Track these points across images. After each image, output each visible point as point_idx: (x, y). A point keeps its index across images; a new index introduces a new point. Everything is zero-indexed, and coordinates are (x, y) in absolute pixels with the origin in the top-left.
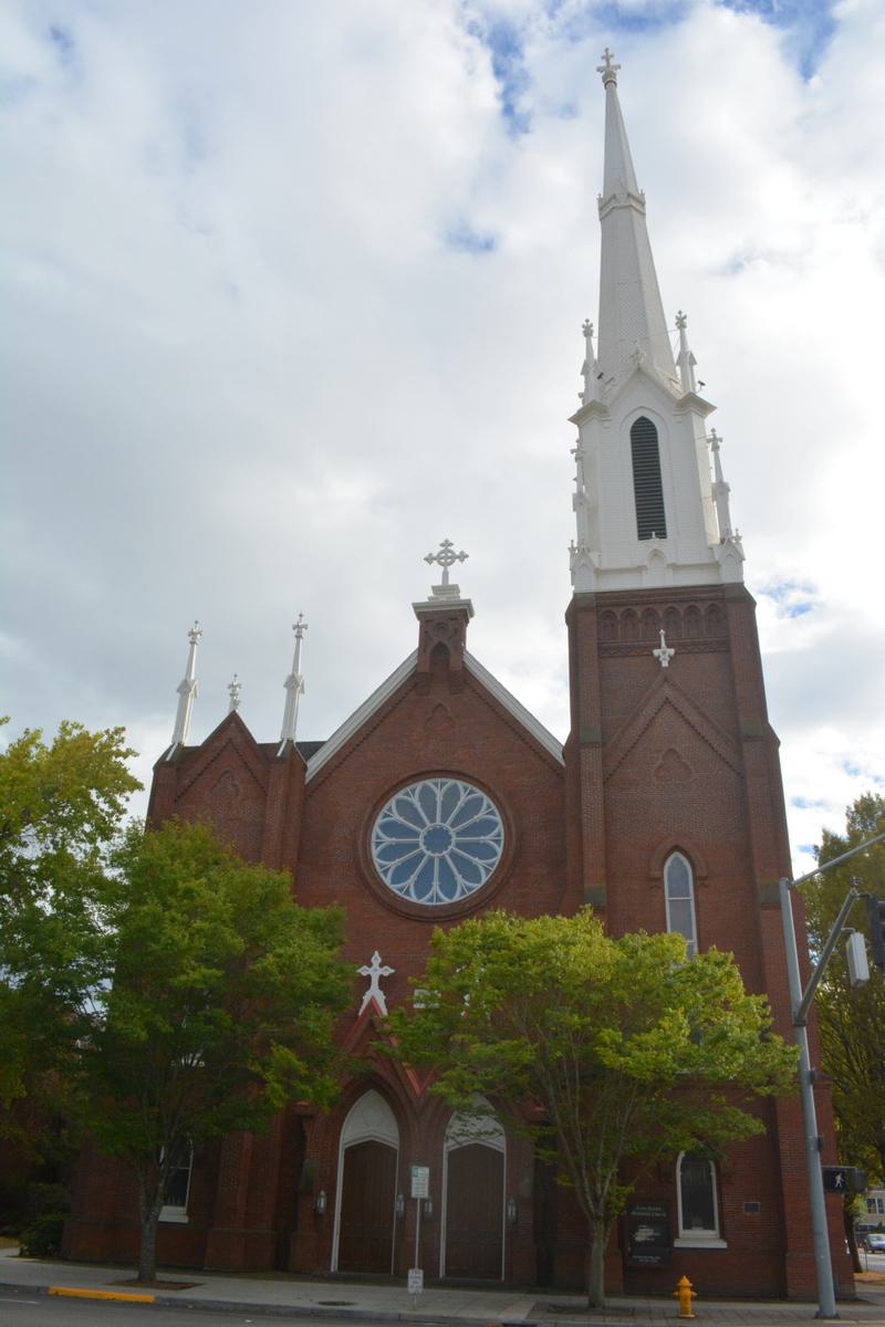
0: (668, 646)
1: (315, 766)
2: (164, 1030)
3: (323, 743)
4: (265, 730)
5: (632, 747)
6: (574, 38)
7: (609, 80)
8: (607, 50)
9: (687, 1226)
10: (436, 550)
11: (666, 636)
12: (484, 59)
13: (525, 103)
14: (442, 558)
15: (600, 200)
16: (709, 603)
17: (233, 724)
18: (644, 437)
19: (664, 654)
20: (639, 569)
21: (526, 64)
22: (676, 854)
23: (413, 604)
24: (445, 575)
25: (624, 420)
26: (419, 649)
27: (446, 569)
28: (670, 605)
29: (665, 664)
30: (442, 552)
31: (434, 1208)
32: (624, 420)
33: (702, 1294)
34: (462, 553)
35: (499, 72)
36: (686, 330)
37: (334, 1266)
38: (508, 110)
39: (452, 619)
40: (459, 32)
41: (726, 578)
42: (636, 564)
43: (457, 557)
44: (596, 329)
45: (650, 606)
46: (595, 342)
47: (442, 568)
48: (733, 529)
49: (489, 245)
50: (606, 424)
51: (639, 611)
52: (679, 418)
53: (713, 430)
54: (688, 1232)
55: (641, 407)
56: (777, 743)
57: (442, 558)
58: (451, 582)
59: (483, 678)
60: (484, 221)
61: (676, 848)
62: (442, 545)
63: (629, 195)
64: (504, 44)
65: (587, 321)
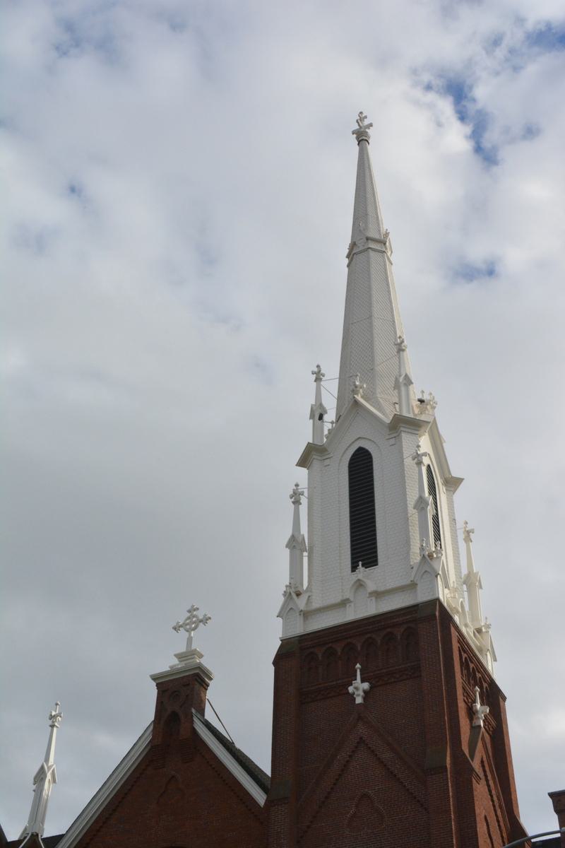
0: (363, 681)
3: (60, 837)
5: (326, 798)
6: (516, 69)
10: (182, 617)
12: (446, 106)
13: (492, 137)
14: (188, 624)
16: (405, 626)
18: (361, 466)
19: (359, 688)
20: (344, 603)
21: (479, 106)
23: (151, 676)
24: (190, 640)
26: (154, 721)
27: (190, 634)
28: (369, 635)
29: (359, 700)
30: (189, 618)
32: (342, 456)
35: (462, 117)
38: (478, 149)
39: (184, 686)
40: (418, 93)
41: (422, 597)
42: (338, 599)
43: (201, 621)
45: (349, 640)
47: (187, 633)
49: (491, 272)
50: (327, 462)
51: (339, 648)
52: (392, 441)
55: (360, 438)
57: (188, 624)
58: (193, 648)
59: (218, 745)
60: (477, 252)
62: (189, 611)
63: (368, 239)
64: (458, 91)
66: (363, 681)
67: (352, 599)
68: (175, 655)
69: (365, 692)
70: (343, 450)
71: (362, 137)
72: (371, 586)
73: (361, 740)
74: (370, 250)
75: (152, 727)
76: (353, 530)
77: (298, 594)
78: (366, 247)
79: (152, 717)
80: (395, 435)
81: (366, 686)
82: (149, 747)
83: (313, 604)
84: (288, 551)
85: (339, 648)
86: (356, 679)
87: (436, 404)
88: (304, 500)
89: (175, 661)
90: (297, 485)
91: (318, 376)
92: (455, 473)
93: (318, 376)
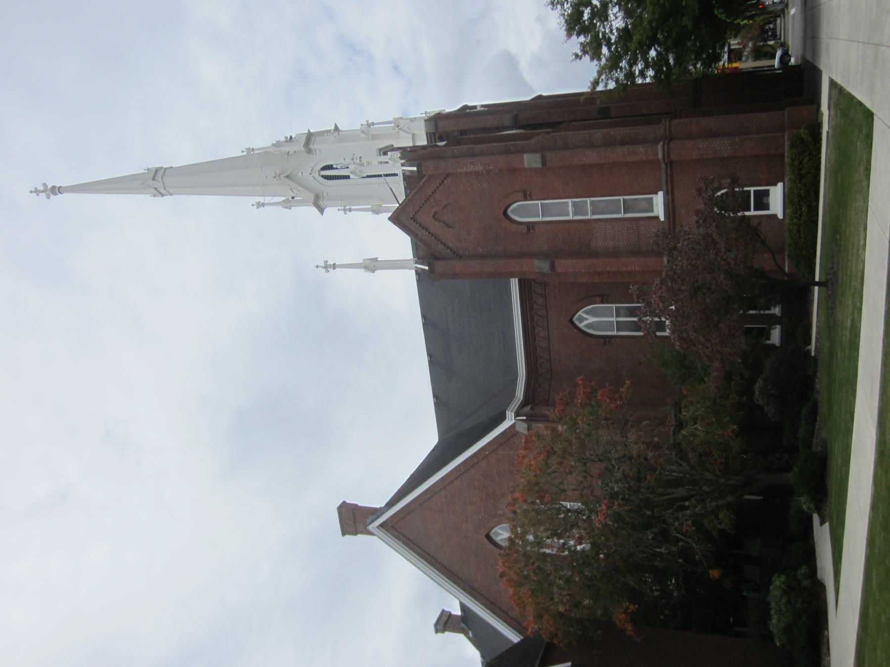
7: (56, 190)
8: (31, 192)
15: (154, 196)
22: (509, 211)
25: (322, 184)
31: (786, 336)
36: (375, 122)
44: (261, 199)
46: (268, 199)
48: (144, 171)
50: (325, 194)
53: (145, 170)
56: (540, 97)
61: (505, 213)
65: (253, 205)
71: (56, 190)
74: (163, 178)
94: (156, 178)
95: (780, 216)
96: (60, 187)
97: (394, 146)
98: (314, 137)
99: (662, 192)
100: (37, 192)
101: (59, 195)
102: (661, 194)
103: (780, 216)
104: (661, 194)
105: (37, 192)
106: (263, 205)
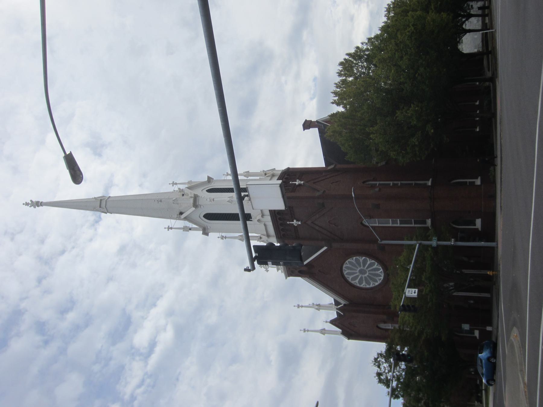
0: (293, 221)
1: (343, 301)
2: (342, 149)
4: (333, 315)
7: (38, 204)
9: (475, 225)
11: (289, 222)
17: (333, 322)
18: (210, 217)
29: (300, 223)
33: (491, 324)
34: (268, 270)
37: (487, 295)
50: (209, 227)
51: (281, 228)
54: (477, 226)
55: (199, 217)
66: (293, 221)
67: (264, 223)
68: (278, 271)
69: (297, 221)
70: (202, 220)
71: (38, 204)
72: (259, 217)
73: (312, 222)
74: (106, 207)
75: (303, 278)
76: (236, 219)
77: (261, 238)
78: (105, 208)
79: (300, 278)
80: (199, 206)
81: (295, 221)
82: (310, 278)
83: (264, 233)
84: (320, 310)
85: (281, 228)
86: (293, 224)
87: (376, 359)
88: (224, 234)
89: (280, 271)
90: (218, 237)
91: (169, 228)
92: (206, 179)
93: (169, 228)
94: (101, 206)
95: (480, 229)
96: (42, 202)
97: (243, 201)
98: (198, 198)
99: (463, 325)
100: (27, 204)
101: (41, 207)
102: (430, 220)
103: (480, 229)
104: (430, 220)
105: (27, 204)
106: (226, 238)
